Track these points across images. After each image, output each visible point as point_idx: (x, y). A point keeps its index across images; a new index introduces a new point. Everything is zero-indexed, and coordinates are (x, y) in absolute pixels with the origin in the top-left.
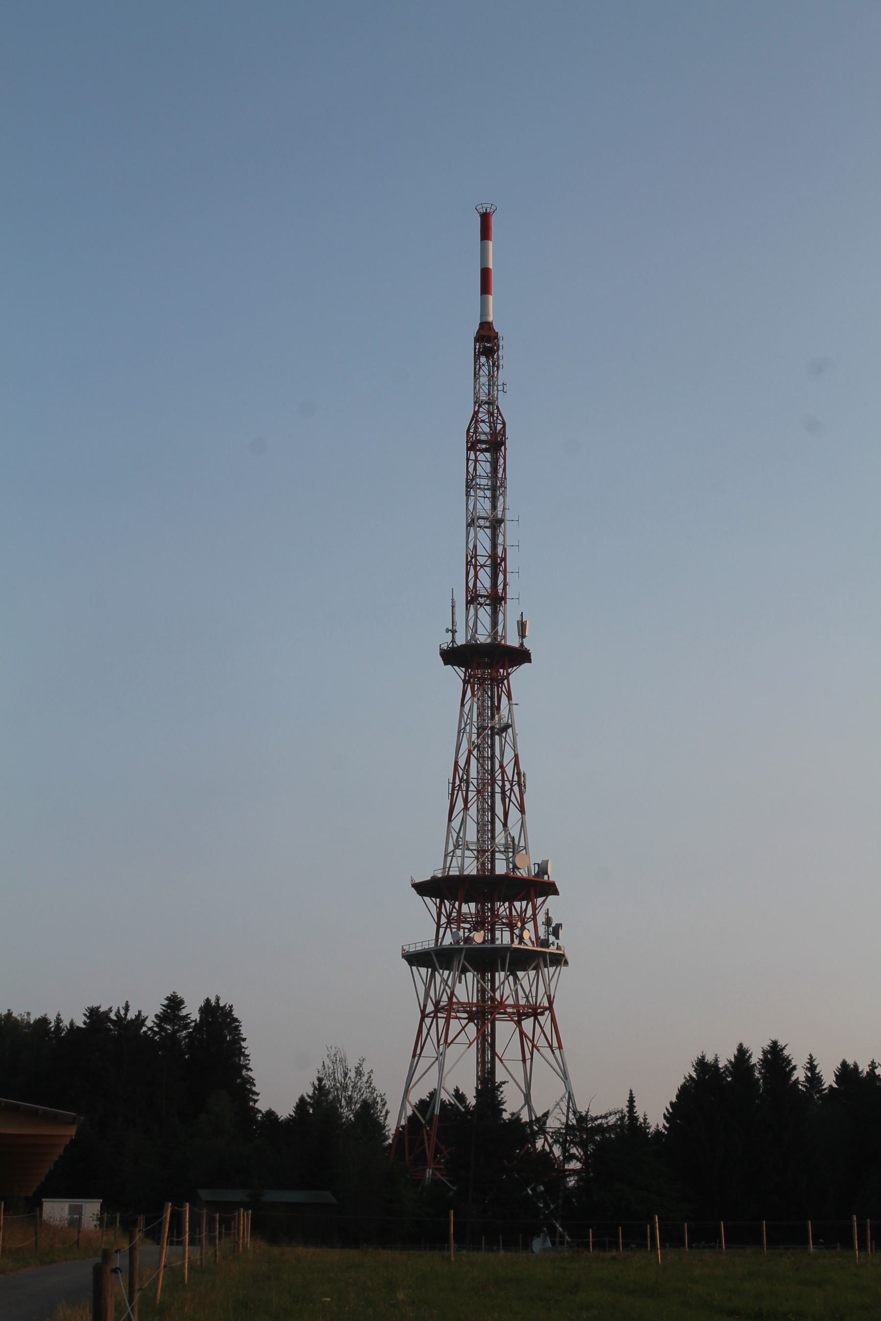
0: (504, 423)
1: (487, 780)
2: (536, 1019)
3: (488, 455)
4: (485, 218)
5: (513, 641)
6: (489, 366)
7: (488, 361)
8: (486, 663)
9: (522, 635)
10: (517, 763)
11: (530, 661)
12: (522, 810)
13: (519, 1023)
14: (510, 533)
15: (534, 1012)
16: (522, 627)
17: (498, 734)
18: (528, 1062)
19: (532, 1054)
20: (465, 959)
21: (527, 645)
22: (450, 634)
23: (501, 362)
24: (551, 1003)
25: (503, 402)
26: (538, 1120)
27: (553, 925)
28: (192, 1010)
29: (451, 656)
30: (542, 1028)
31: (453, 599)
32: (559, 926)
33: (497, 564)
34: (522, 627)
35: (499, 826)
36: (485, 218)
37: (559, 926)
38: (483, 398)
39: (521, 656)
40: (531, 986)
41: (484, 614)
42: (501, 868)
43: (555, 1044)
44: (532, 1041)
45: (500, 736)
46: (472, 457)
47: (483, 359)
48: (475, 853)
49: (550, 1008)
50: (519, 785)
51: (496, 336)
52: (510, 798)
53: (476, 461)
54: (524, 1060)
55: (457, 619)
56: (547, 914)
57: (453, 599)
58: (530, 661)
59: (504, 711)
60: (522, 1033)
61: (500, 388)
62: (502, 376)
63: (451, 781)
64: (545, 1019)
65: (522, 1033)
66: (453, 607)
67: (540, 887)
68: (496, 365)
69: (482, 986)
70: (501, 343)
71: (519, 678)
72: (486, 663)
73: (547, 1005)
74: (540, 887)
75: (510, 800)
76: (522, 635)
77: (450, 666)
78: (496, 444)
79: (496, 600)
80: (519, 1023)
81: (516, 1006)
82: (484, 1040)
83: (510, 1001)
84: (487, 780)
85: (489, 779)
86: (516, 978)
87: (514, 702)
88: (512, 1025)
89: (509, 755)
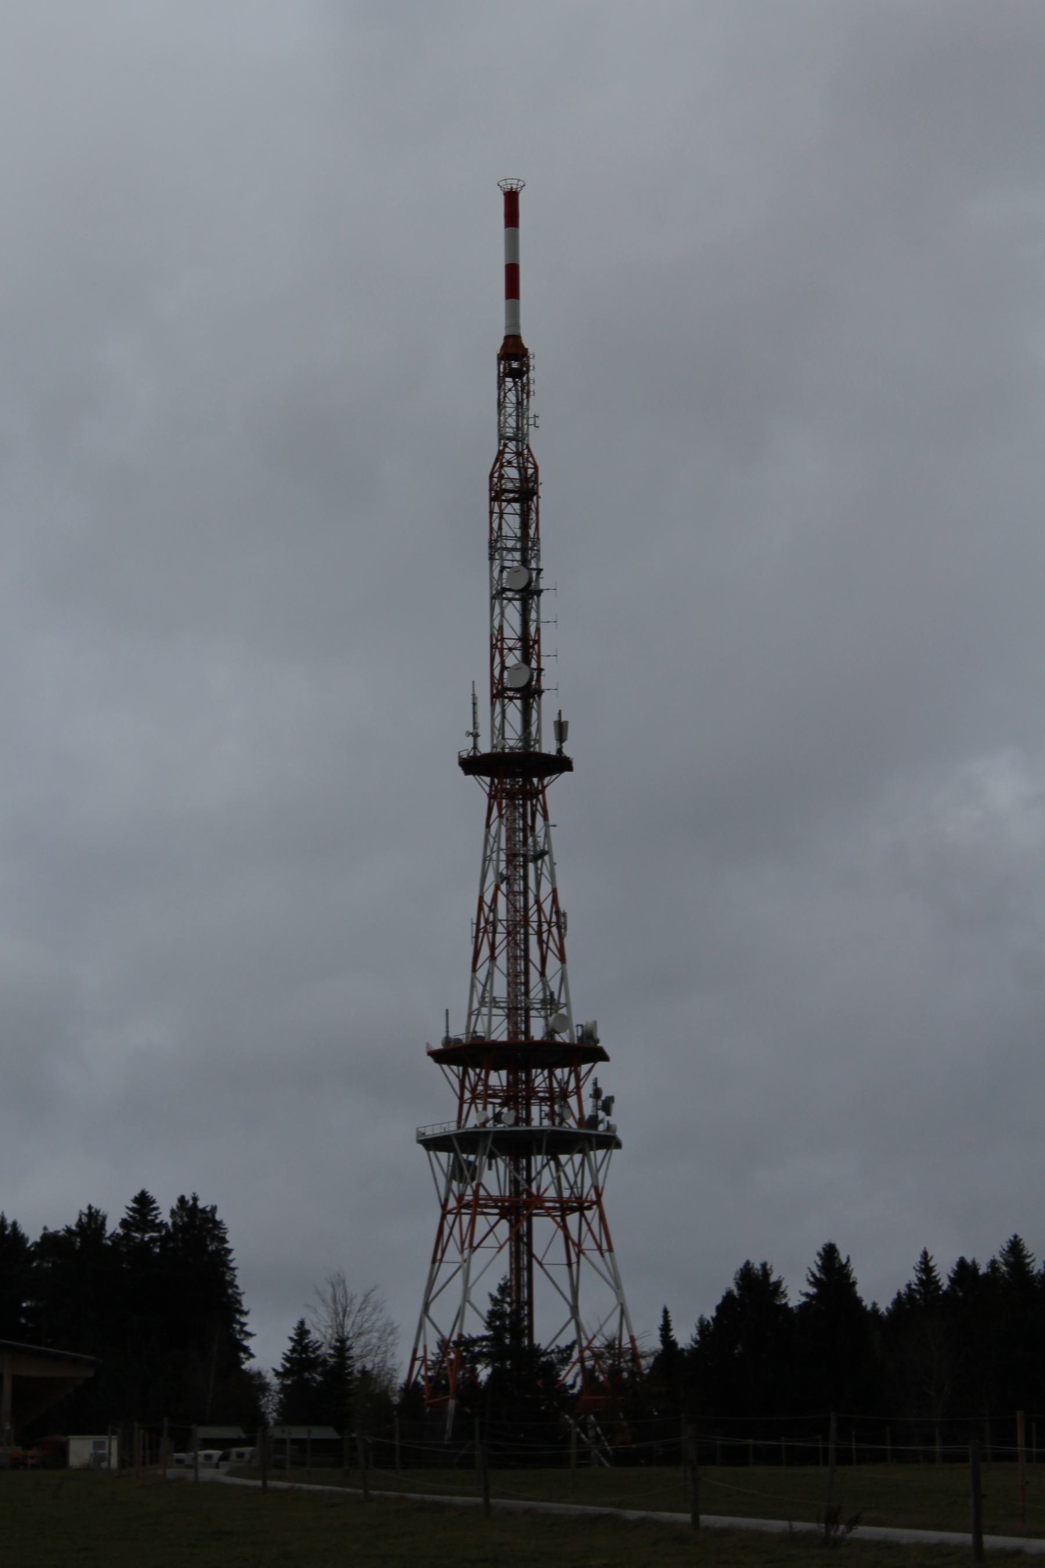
2: (582, 1215)
3: (517, 506)
4: (512, 199)
7: (515, 383)
15: (580, 1206)
16: (561, 730)
20: (493, 1142)
22: (471, 738)
24: (599, 1195)
27: (603, 1098)
29: (472, 765)
31: (474, 695)
32: (610, 1100)
33: (528, 645)
34: (561, 730)
35: (534, 976)
36: (512, 199)
37: (610, 1100)
39: (561, 764)
40: (576, 1175)
41: (514, 711)
46: (496, 509)
49: (598, 1202)
52: (547, 943)
57: (474, 695)
61: (531, 421)
63: (475, 921)
64: (591, 1214)
66: (474, 704)
71: (557, 790)
72: (515, 775)
73: (594, 1198)
78: (526, 493)
79: (530, 694)
84: (519, 923)
85: (519, 924)
86: (559, 1165)
89: (546, 889)
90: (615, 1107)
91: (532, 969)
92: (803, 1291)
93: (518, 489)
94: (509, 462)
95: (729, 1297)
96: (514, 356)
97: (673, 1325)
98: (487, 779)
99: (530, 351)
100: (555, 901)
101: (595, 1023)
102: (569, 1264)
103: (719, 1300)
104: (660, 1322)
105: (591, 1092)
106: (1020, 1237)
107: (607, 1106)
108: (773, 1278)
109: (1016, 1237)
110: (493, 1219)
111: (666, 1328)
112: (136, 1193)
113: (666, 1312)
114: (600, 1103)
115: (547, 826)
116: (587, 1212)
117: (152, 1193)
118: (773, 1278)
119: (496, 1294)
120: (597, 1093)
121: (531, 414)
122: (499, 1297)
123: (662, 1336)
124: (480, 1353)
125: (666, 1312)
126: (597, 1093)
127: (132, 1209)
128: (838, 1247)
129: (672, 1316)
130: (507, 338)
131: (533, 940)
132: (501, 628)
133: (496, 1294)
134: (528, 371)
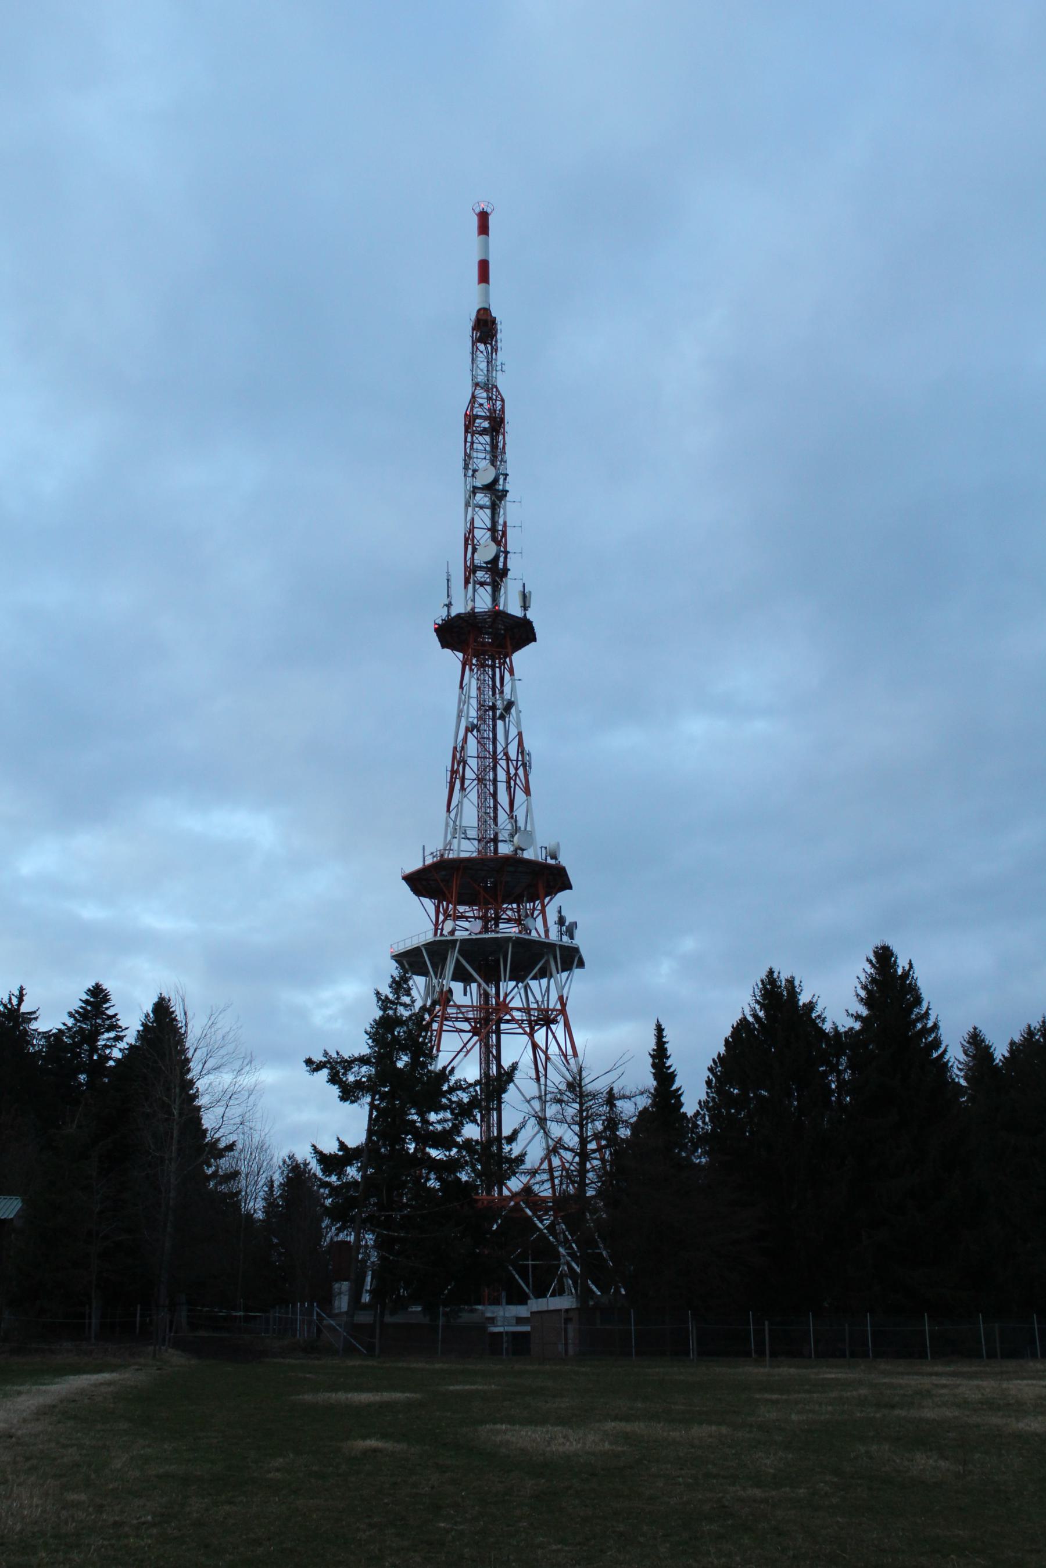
0: (503, 400)
1: (489, 759)
2: (549, 1027)
3: (488, 438)
4: (483, 219)
5: (514, 609)
6: (487, 352)
8: (487, 638)
9: (525, 607)
10: (521, 744)
11: (568, 886)
12: (527, 791)
13: (531, 1035)
14: (511, 512)
15: (546, 1020)
16: (525, 600)
17: (502, 717)
18: (542, 1080)
19: (546, 1069)
20: (459, 952)
21: (530, 615)
22: (446, 608)
23: (499, 345)
24: (564, 1005)
25: (502, 382)
26: (557, 1143)
27: (567, 924)
28: (131, 1016)
30: (555, 1037)
31: (448, 572)
32: (574, 925)
33: (498, 535)
34: (525, 600)
35: (502, 816)
36: (483, 219)
37: (574, 925)
38: (481, 379)
40: (543, 997)
42: (504, 849)
43: (570, 1052)
44: (546, 1053)
45: (504, 721)
46: (469, 439)
47: (481, 347)
48: (476, 843)
49: (563, 1011)
50: (524, 765)
51: (494, 321)
52: (515, 781)
53: (472, 443)
54: (538, 1079)
55: (453, 592)
56: (560, 912)
57: (448, 572)
58: (568, 886)
59: (507, 689)
60: (535, 1046)
61: (499, 368)
62: (500, 357)
64: (559, 1029)
65: (535, 1046)
66: (448, 580)
67: (552, 878)
68: (495, 350)
69: (485, 990)
70: (499, 327)
72: (487, 638)
73: (559, 1007)
74: (552, 878)
75: (515, 784)
76: (525, 607)
77: (449, 651)
78: (496, 424)
79: (497, 572)
80: (531, 1035)
81: (527, 1010)
82: (488, 1052)
83: (516, 1003)
84: (489, 759)
85: (491, 759)
86: (527, 987)
87: (517, 676)
88: (526, 1038)
89: (513, 732)
90: (577, 933)
91: (500, 810)
92: (852, 1011)
93: (488, 422)
94: (481, 405)
95: (742, 1027)
96: (485, 328)
97: (670, 1048)
98: (460, 655)
99: (498, 320)
100: (521, 744)
101: (558, 844)
102: (538, 1079)
103: (728, 1032)
104: (652, 1044)
105: (556, 919)
106: (980, 1028)
107: (570, 932)
108: (804, 999)
109: (975, 1029)
110: (466, 1036)
111: (660, 1054)
112: (90, 984)
113: (660, 1030)
114: (564, 928)
115: (513, 680)
116: (552, 1026)
117: (106, 985)
118: (804, 999)
119: (386, 991)
120: (561, 921)
121: (498, 363)
122: (391, 996)
123: (654, 1065)
124: (358, 1084)
125: (660, 1030)
126: (561, 921)
127: (86, 1002)
128: (895, 949)
129: (669, 1035)
130: (479, 311)
131: (502, 788)
132: (473, 519)
133: (386, 991)
134: (495, 335)
